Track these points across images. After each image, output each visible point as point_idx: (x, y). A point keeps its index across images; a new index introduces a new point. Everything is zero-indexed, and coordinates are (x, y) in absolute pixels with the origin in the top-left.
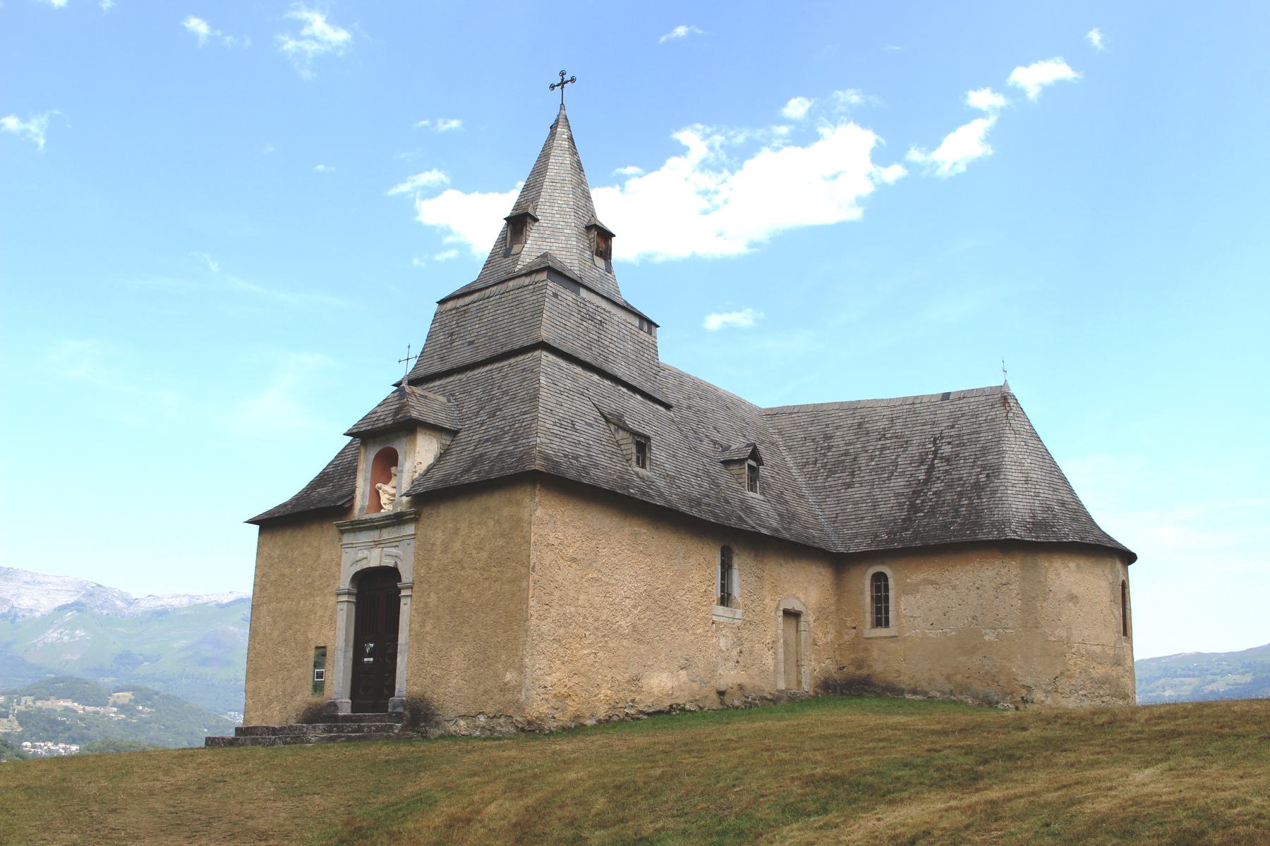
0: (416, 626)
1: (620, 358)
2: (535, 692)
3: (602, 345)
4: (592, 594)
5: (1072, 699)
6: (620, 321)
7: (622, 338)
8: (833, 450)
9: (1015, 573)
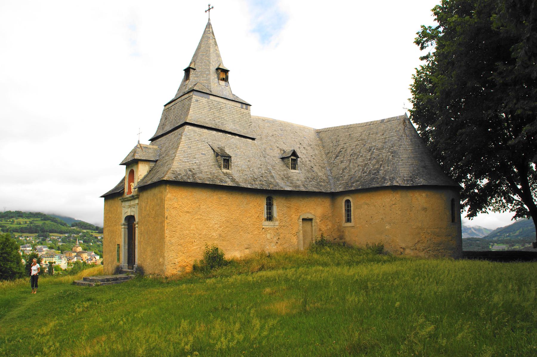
0: (139, 238)
3: (220, 118)
4: (197, 225)
7: (231, 113)
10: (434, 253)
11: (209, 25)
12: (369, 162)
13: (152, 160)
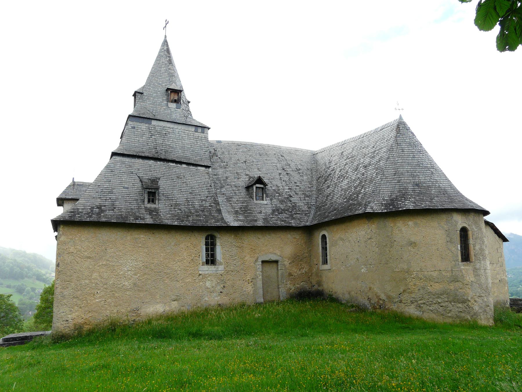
9: (374, 232)
11: (165, 43)
13: (71, 198)
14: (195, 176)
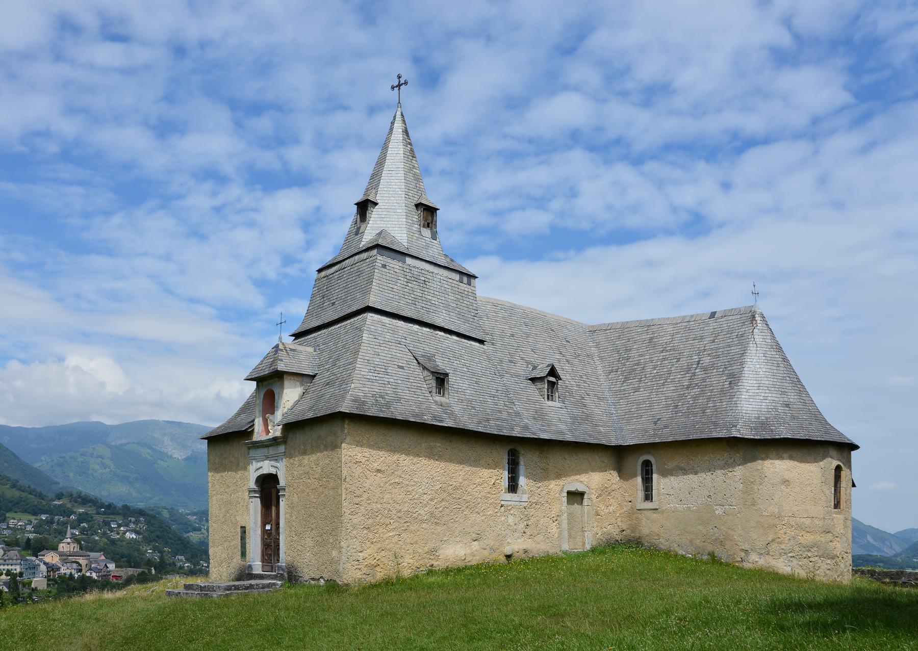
1: (442, 308)
2: (350, 564)
3: (425, 299)
5: (782, 560)
6: (442, 278)
8: (631, 360)
10: (800, 563)
12: (687, 392)
14: (473, 356)
